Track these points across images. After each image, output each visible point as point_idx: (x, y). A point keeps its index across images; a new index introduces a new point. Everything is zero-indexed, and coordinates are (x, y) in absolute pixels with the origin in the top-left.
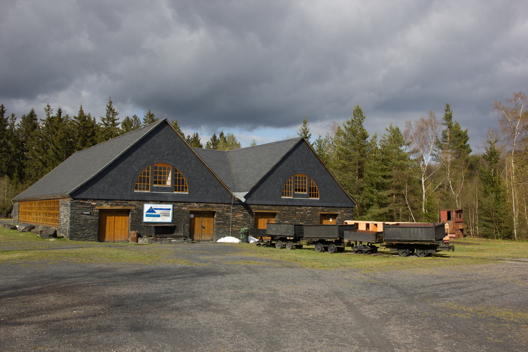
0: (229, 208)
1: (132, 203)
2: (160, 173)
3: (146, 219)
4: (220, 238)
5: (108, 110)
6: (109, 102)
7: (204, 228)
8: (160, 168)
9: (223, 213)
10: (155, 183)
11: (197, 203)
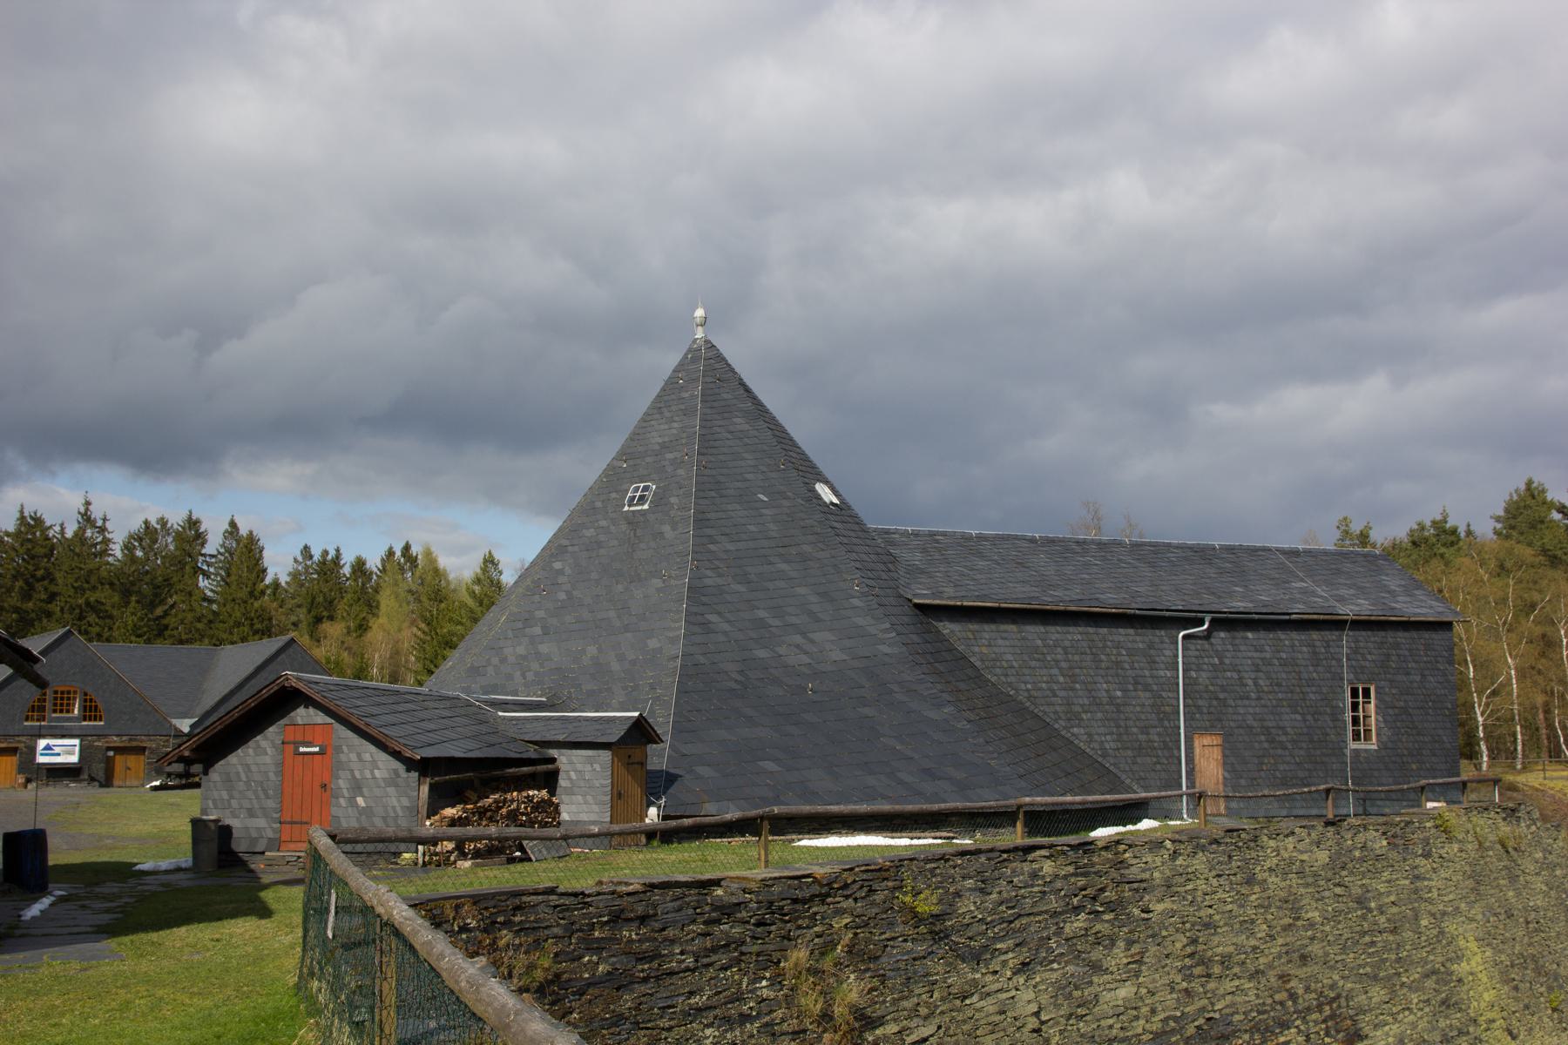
0: (168, 741)
1: (20, 738)
2: (69, 699)
3: (41, 759)
4: (1094, 829)
5: (81, 520)
7: (129, 769)
8: (62, 693)
9: (157, 749)
10: (55, 711)
11: (117, 736)
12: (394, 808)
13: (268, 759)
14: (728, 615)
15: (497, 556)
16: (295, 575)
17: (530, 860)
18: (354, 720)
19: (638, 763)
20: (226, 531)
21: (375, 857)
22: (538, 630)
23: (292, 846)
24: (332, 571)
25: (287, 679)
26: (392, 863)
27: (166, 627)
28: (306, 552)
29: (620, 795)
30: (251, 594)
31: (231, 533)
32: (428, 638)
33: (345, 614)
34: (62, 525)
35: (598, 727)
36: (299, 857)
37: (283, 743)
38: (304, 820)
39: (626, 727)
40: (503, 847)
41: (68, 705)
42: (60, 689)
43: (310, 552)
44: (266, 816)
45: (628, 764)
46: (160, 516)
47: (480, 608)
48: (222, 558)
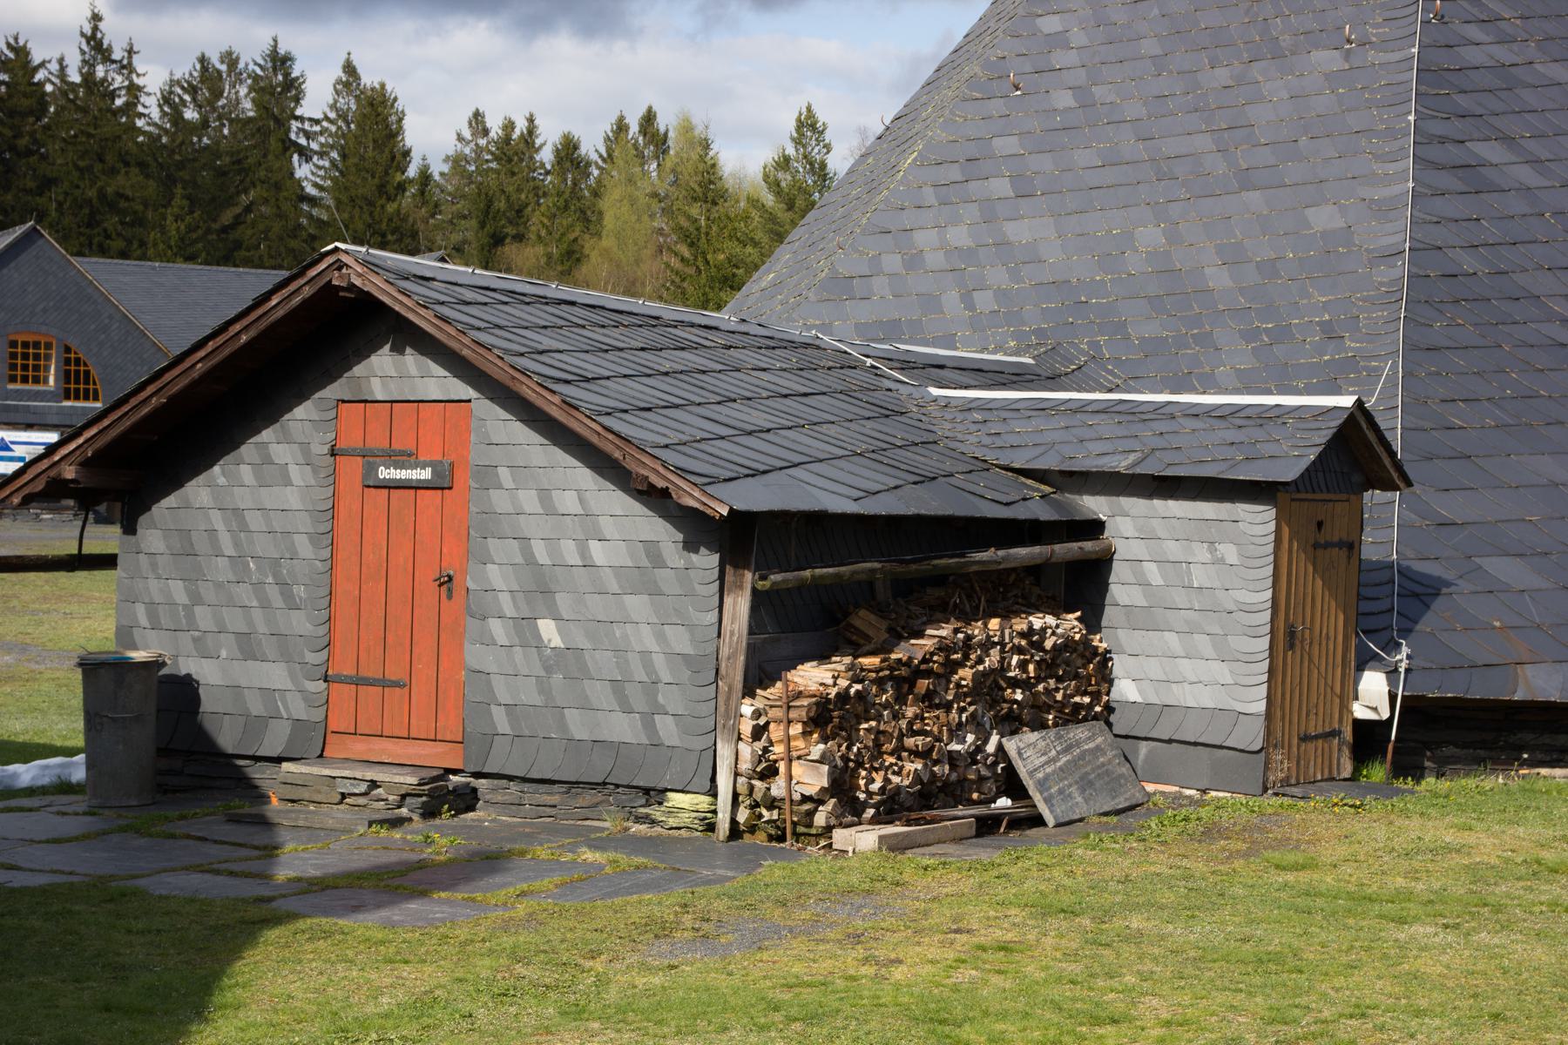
2: (37, 357)
6: (89, 14)
8: (26, 345)
12: (645, 655)
13: (292, 498)
14: (1534, 147)
15: (822, 117)
16: (457, 161)
17: (1038, 821)
18: (528, 391)
19: (1340, 544)
20: (339, 81)
21: (589, 797)
22: (1001, 187)
23: (358, 748)
24: (520, 155)
25: (340, 266)
26: (639, 819)
27: (238, 245)
28: (477, 118)
29: (1291, 634)
30: (381, 188)
31: (347, 85)
32: (691, 271)
33: (543, 233)
34: (61, 61)
35: (1231, 435)
36: (374, 784)
37: (333, 453)
38: (393, 673)
39: (1323, 437)
40: (963, 781)
41: (36, 368)
42: (21, 339)
43: (483, 123)
44: (286, 657)
45: (1316, 546)
46: (224, 49)
47: (789, 215)
48: (333, 129)
